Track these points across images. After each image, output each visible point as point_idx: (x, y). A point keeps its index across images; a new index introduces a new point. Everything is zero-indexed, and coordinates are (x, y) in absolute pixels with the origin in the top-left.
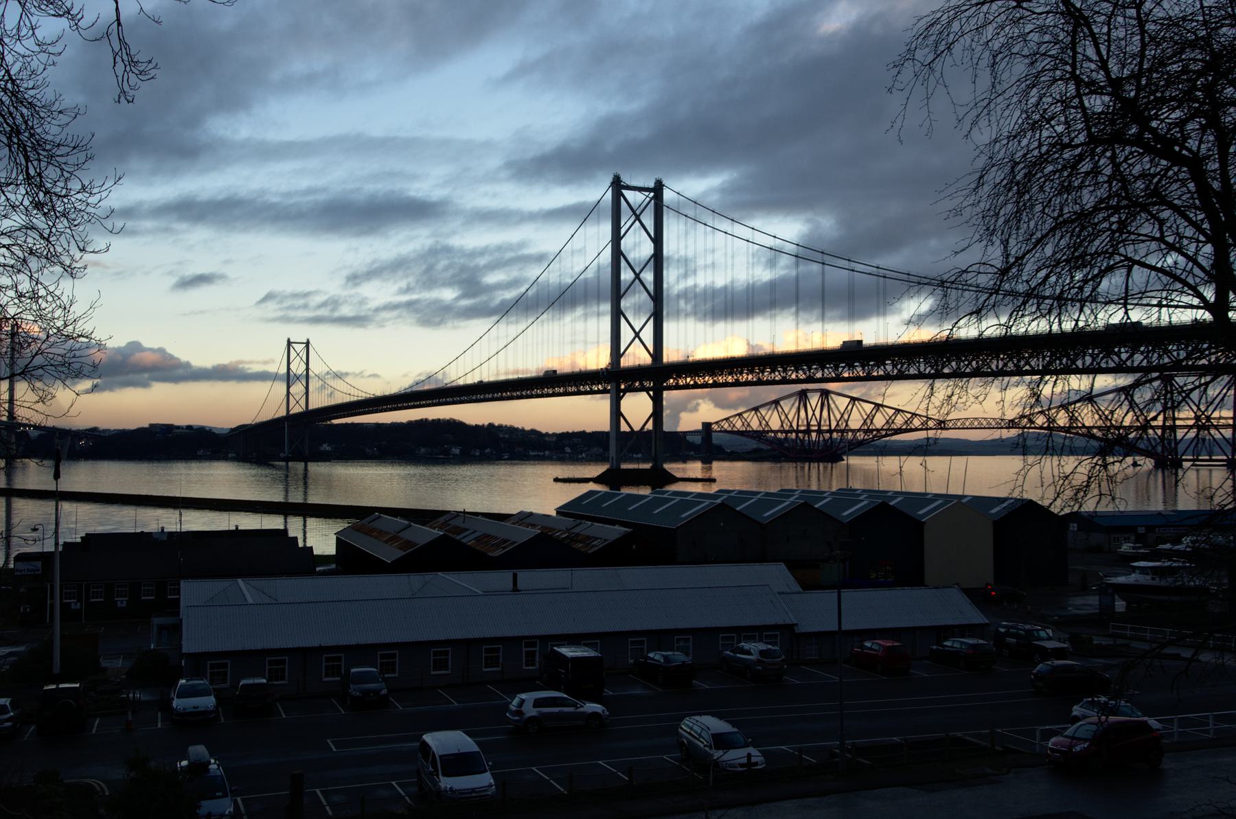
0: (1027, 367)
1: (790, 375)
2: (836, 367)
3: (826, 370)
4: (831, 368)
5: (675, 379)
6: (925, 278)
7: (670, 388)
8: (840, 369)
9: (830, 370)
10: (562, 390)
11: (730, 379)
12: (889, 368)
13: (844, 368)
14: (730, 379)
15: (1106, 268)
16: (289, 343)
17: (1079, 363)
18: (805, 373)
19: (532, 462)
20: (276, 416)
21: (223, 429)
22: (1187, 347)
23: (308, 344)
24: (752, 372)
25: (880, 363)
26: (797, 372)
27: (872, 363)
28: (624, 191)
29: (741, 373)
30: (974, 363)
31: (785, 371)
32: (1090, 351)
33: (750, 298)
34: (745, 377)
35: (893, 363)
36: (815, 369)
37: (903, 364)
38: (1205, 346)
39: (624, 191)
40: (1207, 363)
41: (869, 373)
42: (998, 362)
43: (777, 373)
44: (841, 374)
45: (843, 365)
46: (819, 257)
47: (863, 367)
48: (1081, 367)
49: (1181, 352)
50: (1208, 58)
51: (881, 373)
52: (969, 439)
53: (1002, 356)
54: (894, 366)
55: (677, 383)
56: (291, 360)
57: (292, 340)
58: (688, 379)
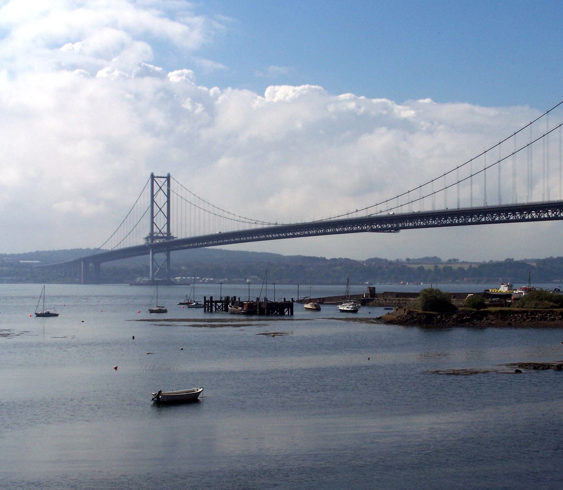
1: (455, 221)
2: (507, 215)
3: (487, 217)
4: (504, 215)
8: (509, 216)
9: (503, 216)
10: (307, 233)
11: (307, 233)
12: (550, 214)
13: (510, 215)
15: (303, 235)
16: (153, 177)
17: (470, 221)
18: (462, 219)
19: (363, 218)
20: (116, 248)
21: (88, 250)
23: (168, 178)
24: (434, 219)
25: (529, 212)
26: (459, 219)
27: (541, 211)
28: (155, 178)
29: (406, 222)
31: (452, 219)
33: (530, 176)
35: (552, 211)
36: (481, 216)
37: (557, 212)
39: (155, 178)
41: (539, 216)
43: (448, 220)
44: (509, 218)
45: (510, 213)
47: (521, 214)
50: (365, 224)
51: (530, 217)
52: (539, 258)
54: (553, 213)
56: (155, 193)
57: (155, 175)
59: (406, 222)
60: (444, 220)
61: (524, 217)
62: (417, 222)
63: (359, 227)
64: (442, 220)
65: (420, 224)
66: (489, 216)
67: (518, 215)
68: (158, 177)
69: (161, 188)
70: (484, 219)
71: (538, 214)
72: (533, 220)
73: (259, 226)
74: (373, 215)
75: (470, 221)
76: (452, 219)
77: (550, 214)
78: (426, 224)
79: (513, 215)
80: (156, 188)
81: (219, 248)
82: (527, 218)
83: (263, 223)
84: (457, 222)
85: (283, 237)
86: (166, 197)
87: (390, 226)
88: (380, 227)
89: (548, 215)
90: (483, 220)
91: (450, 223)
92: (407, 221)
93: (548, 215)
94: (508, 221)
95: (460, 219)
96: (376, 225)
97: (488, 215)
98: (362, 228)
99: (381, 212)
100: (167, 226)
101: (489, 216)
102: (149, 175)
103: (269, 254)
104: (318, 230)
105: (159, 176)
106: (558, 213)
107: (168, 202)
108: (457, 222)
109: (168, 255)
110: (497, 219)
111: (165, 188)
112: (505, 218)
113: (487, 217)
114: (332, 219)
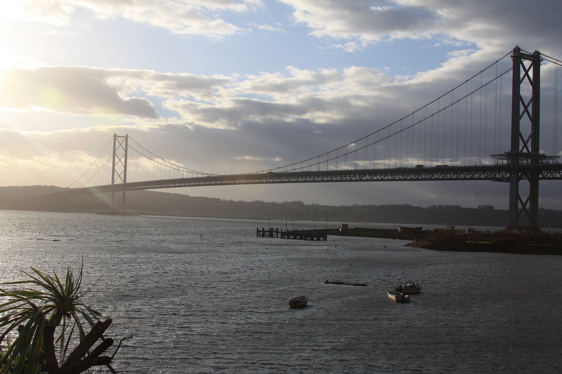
0: (446, 177)
1: (308, 179)
3: (328, 178)
5: (233, 181)
6: (212, 175)
7: (544, 178)
9: (338, 177)
10: (198, 184)
11: (198, 184)
14: (271, 180)
16: (115, 136)
17: (476, 176)
18: (312, 179)
20: (81, 187)
22: (547, 172)
23: (127, 137)
24: (294, 178)
28: (117, 137)
30: (417, 176)
31: (306, 178)
32: (502, 172)
34: (292, 180)
36: (333, 177)
38: (552, 172)
39: (117, 137)
40: (552, 177)
42: (477, 175)
43: (303, 179)
44: (333, 179)
46: (192, 172)
48: (436, 178)
49: (545, 173)
52: (57, 185)
53: (439, 174)
54: (380, 176)
55: (240, 182)
56: (120, 138)
57: (117, 135)
58: (244, 181)
59: (269, 179)
60: (300, 178)
61: (361, 179)
62: (276, 179)
63: (238, 181)
64: (299, 179)
65: (285, 180)
66: (329, 177)
67: (348, 177)
68: (119, 137)
69: (120, 160)
70: (507, 175)
71: (371, 177)
72: (367, 180)
73: (200, 176)
74: (258, 173)
75: (317, 180)
76: (306, 178)
77: (368, 177)
78: (289, 180)
79: (355, 177)
80: (117, 144)
81: (153, 191)
82: (353, 179)
83: (202, 173)
84: (309, 180)
85: (197, 185)
86: (124, 151)
87: (258, 181)
88: (252, 182)
89: (377, 178)
90: (326, 179)
91: (442, 178)
92: (424, 174)
93: (377, 178)
94: (351, 180)
95: (311, 178)
96: (237, 181)
97: (338, 176)
98: (246, 182)
99: (295, 170)
100: (124, 173)
101: (329, 177)
102: (113, 135)
103: (289, 203)
104: (211, 182)
105: (120, 136)
106: (383, 177)
107: (114, 150)
108: (309, 180)
109: (124, 194)
110: (335, 179)
111: (124, 145)
112: (339, 179)
113: (328, 178)
114: (288, 172)
